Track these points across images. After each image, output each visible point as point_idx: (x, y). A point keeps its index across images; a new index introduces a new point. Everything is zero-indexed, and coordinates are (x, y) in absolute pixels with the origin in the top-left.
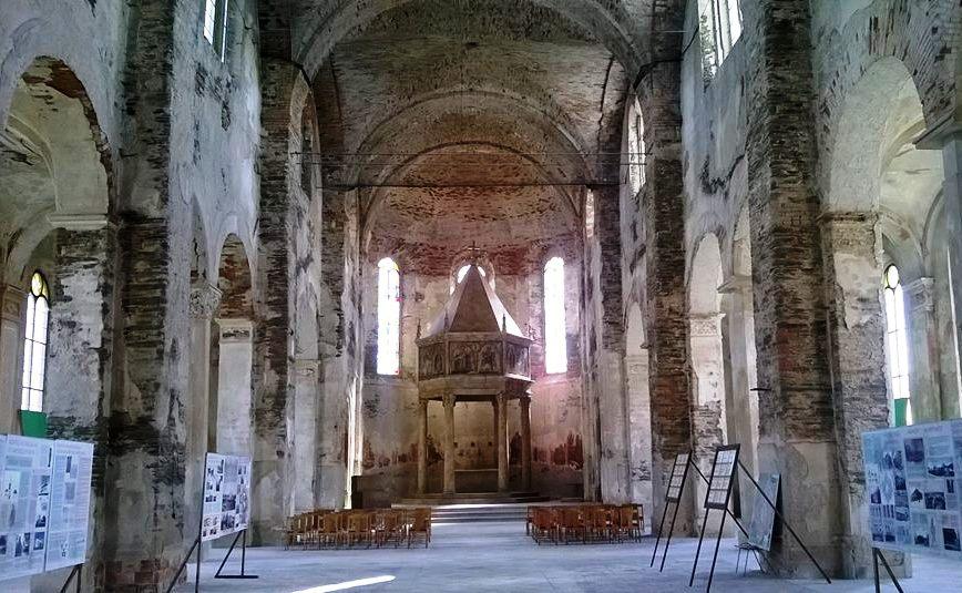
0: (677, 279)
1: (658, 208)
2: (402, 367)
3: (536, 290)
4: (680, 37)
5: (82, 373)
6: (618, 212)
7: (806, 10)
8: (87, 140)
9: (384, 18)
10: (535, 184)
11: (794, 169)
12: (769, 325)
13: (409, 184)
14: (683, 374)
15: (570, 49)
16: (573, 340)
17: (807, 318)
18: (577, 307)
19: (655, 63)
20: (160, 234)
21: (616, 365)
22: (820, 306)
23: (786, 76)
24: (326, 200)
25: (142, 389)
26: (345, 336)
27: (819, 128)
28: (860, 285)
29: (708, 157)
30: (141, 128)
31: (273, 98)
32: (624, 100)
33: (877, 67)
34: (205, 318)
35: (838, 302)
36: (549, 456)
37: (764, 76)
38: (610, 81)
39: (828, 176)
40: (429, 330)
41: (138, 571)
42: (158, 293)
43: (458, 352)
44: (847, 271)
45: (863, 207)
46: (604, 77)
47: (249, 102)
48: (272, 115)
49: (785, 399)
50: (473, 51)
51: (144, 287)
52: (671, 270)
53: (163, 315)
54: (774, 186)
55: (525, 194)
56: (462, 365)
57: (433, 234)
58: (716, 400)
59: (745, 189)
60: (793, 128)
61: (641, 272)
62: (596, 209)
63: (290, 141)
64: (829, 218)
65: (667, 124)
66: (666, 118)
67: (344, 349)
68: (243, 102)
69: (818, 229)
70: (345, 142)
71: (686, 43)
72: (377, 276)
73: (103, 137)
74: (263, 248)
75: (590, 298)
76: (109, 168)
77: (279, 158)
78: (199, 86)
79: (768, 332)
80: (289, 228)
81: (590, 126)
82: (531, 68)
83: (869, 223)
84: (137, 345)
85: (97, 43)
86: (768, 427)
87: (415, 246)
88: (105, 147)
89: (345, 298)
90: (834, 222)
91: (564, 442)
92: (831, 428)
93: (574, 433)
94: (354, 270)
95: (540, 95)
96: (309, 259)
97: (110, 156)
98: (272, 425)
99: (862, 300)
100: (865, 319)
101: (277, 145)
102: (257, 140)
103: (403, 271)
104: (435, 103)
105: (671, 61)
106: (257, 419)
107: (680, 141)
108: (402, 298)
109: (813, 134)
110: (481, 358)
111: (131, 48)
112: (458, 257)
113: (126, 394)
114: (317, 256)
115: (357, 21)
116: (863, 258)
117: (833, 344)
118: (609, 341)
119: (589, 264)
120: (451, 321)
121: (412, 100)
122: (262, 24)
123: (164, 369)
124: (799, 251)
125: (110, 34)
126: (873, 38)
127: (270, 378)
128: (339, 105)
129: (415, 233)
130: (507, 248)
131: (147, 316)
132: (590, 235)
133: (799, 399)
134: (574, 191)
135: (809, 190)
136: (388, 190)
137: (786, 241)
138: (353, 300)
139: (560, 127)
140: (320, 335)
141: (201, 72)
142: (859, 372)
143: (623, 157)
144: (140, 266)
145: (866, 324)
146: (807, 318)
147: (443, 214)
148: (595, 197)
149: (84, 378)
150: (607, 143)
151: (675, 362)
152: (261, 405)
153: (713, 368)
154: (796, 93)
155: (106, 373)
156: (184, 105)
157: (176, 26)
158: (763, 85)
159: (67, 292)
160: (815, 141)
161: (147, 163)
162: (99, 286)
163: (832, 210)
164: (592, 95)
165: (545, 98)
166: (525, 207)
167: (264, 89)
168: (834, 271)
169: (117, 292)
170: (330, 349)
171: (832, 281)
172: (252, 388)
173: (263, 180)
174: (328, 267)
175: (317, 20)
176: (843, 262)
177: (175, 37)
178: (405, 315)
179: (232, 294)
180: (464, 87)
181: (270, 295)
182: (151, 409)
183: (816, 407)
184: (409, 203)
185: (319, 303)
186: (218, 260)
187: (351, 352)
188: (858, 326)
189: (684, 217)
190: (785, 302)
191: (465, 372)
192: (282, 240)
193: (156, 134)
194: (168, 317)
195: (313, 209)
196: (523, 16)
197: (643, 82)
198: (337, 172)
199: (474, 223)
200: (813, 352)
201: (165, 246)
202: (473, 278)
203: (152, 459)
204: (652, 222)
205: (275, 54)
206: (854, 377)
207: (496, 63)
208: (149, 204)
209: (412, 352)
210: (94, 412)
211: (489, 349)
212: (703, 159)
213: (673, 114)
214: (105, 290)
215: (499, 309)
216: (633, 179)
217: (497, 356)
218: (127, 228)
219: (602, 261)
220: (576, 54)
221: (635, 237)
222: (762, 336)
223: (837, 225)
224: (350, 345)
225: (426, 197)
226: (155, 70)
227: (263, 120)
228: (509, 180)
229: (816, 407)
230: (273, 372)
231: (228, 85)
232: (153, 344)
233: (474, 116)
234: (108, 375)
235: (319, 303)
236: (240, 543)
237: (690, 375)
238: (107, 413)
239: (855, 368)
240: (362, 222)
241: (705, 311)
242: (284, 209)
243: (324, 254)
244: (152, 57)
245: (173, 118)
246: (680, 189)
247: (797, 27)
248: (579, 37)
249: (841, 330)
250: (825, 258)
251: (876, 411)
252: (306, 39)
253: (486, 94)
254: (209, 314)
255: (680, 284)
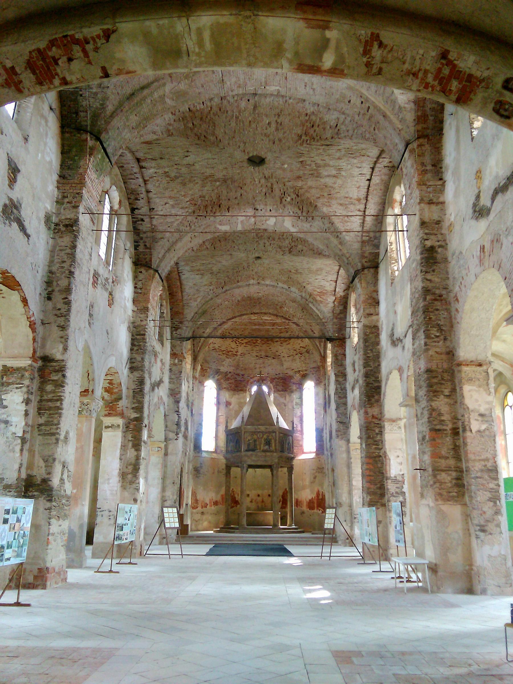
0: (376, 397)
1: (365, 353)
2: (217, 446)
3: (298, 401)
4: (377, 255)
5: (10, 451)
6: (345, 355)
7: (445, 240)
8: (22, 315)
9: (206, 244)
10: (298, 337)
11: (438, 334)
12: (424, 429)
13: (223, 337)
14: (380, 456)
15: (315, 260)
16: (319, 432)
17: (447, 426)
18: (322, 412)
19: (363, 268)
20: (61, 370)
21: (344, 448)
22: (455, 419)
23: (433, 279)
24: (173, 347)
25: (46, 461)
26: (181, 426)
27: (453, 310)
28: (480, 405)
29: (393, 325)
30: (54, 308)
31: (141, 289)
32: (349, 287)
33: (484, 274)
34: (92, 417)
35: (466, 416)
36: (305, 504)
37: (419, 278)
38: (339, 278)
39: (459, 338)
40: (235, 424)
41: (36, 574)
42: (58, 404)
43: (249, 438)
44: (471, 396)
45: (481, 358)
46: (336, 276)
47: (126, 291)
48: (140, 298)
49: (435, 476)
50: (259, 261)
51: (50, 400)
52: (373, 392)
53: (60, 417)
54: (426, 344)
55: (291, 344)
56: (252, 446)
57: (237, 366)
58: (402, 473)
59: (411, 346)
60: (437, 310)
61: (357, 391)
62: (332, 353)
63: (149, 314)
64: (459, 365)
65: (371, 305)
66: (370, 301)
67: (180, 435)
68: (122, 292)
69: (453, 371)
70: (185, 313)
71: (381, 257)
72: (203, 391)
73: (31, 313)
74: (130, 375)
75: (329, 407)
76: (34, 330)
77: (143, 323)
78: (95, 283)
79: (424, 434)
80: (146, 364)
81: (327, 307)
82: (293, 271)
83: (485, 367)
84: (44, 435)
85: (30, 259)
86: (425, 493)
87: (226, 374)
88: (32, 319)
89: (182, 404)
90: (463, 366)
91: (314, 495)
92: (463, 495)
93: (321, 490)
94: (189, 387)
95: (299, 286)
96: (161, 381)
97: (35, 324)
98: (131, 483)
99: (481, 415)
100: (484, 427)
101: (141, 316)
102: (130, 313)
103: (220, 388)
104: (237, 291)
105: (372, 268)
106: (123, 479)
107: (378, 314)
108: (218, 403)
109: (450, 313)
110: (263, 441)
111: (51, 262)
112: (252, 380)
113: (36, 464)
114: (166, 379)
115: (190, 245)
116: (481, 389)
117: (464, 442)
118: (339, 433)
119: (328, 386)
120: (245, 419)
121: (224, 289)
122: (136, 247)
123: (59, 450)
124: (441, 384)
125: (38, 254)
126: (482, 257)
127: (131, 453)
128: (182, 292)
129: (227, 366)
130: (281, 375)
131: (52, 417)
132: (329, 368)
133: (444, 477)
134: (320, 342)
135: (448, 347)
136: (211, 340)
137: (434, 377)
138: (188, 406)
139: (311, 305)
140: (166, 427)
141: (96, 276)
142: (480, 460)
143: (347, 324)
144: (49, 388)
145: (484, 430)
146: (447, 426)
147: (243, 354)
148: (332, 346)
149: (11, 454)
150: (338, 314)
151: (376, 448)
152: (126, 470)
153: (399, 453)
154: (439, 289)
155: (24, 451)
156: (83, 294)
157: (78, 250)
158: (419, 284)
159: (5, 403)
160: (451, 318)
161: (57, 328)
162: (24, 399)
163: (461, 359)
164: (329, 287)
165: (302, 288)
166: (292, 351)
167: (136, 284)
168: (463, 397)
169: (34, 404)
170: (172, 435)
171: (462, 403)
172: (121, 459)
173: (133, 335)
174: (173, 386)
175: (167, 245)
176: (469, 391)
177: (77, 256)
178: (220, 414)
179: (111, 403)
180: (255, 282)
181: (134, 403)
182: (49, 473)
183: (454, 481)
184: (223, 348)
185: (166, 407)
186: (102, 381)
187: (185, 437)
188: (479, 431)
189: (380, 359)
190: (433, 415)
191: (253, 450)
192: (142, 371)
193: (62, 311)
194: (63, 419)
195: (165, 353)
196: (287, 242)
197: (356, 280)
198: (179, 330)
199: (261, 360)
200: (452, 447)
201: (64, 376)
202: (260, 392)
203: (48, 505)
204: (361, 363)
205: (142, 263)
206: (477, 464)
207: (272, 268)
208: (56, 353)
209: (223, 436)
210: (15, 475)
211: (268, 436)
212: (391, 325)
213: (374, 299)
214: (27, 402)
215: (274, 410)
216: (354, 336)
217: (273, 441)
218: (43, 366)
219: (336, 384)
220: (319, 263)
221: (355, 370)
222: (421, 436)
223: (465, 368)
224: (185, 433)
225: (233, 345)
226: (64, 275)
227: (134, 301)
228: (282, 335)
229: (454, 481)
230: (133, 450)
231: (113, 282)
232: (53, 434)
233: (260, 298)
234: (26, 453)
235: (166, 407)
236: (110, 555)
237: (385, 457)
238: (24, 476)
239: (477, 458)
240: (195, 359)
241: (394, 417)
242: (144, 353)
243: (170, 378)
244: (62, 267)
245: (73, 302)
246: (378, 343)
247: (440, 250)
248: (320, 254)
249: (468, 434)
250: (458, 390)
251: (492, 485)
252: (160, 256)
253: (267, 285)
254: (94, 415)
255: (378, 401)
